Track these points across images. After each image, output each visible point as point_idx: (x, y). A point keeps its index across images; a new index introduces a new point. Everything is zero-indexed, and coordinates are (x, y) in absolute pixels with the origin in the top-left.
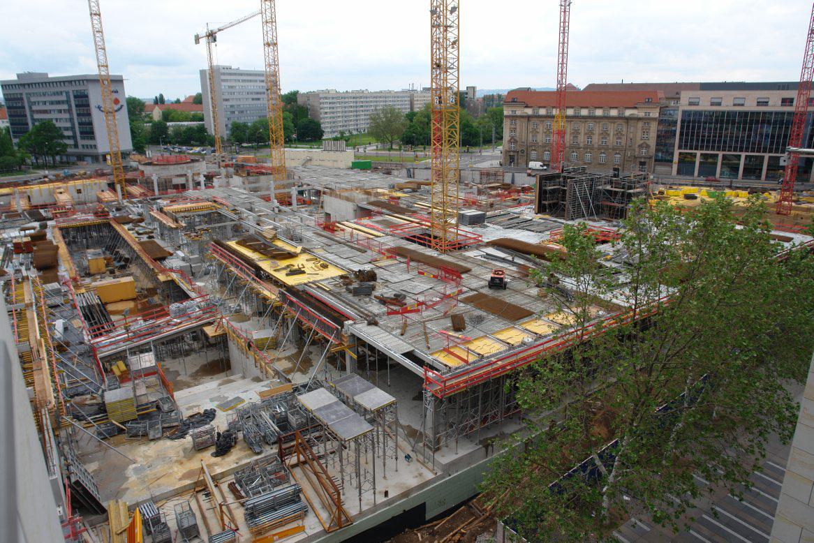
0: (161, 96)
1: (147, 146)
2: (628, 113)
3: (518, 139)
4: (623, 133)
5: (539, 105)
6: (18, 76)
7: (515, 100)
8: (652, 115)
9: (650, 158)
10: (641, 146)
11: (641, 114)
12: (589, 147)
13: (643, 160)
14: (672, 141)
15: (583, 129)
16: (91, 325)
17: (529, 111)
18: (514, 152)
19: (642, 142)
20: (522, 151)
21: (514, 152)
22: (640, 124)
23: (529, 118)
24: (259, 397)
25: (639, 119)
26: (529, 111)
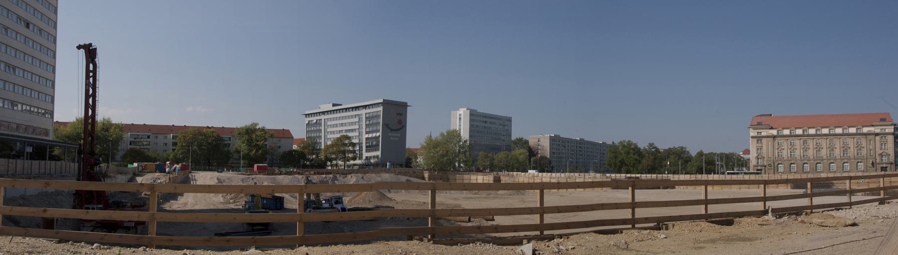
0: (702, 151)
1: (96, 133)
2: (865, 130)
3: (765, 156)
4: (863, 146)
5: (863, 125)
6: (555, 141)
7: (760, 123)
8: (887, 131)
9: (891, 164)
10: (881, 155)
11: (877, 130)
12: (831, 160)
13: (884, 165)
14: (378, 128)
15: (825, 144)
16: (35, 195)
17: (774, 132)
18: (761, 166)
19: (882, 151)
20: (770, 165)
21: (761, 166)
22: (878, 138)
23: (774, 137)
24: (102, 119)
25: (877, 134)
26: (774, 132)
